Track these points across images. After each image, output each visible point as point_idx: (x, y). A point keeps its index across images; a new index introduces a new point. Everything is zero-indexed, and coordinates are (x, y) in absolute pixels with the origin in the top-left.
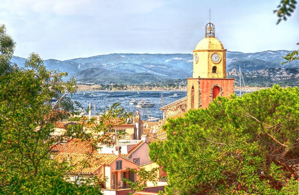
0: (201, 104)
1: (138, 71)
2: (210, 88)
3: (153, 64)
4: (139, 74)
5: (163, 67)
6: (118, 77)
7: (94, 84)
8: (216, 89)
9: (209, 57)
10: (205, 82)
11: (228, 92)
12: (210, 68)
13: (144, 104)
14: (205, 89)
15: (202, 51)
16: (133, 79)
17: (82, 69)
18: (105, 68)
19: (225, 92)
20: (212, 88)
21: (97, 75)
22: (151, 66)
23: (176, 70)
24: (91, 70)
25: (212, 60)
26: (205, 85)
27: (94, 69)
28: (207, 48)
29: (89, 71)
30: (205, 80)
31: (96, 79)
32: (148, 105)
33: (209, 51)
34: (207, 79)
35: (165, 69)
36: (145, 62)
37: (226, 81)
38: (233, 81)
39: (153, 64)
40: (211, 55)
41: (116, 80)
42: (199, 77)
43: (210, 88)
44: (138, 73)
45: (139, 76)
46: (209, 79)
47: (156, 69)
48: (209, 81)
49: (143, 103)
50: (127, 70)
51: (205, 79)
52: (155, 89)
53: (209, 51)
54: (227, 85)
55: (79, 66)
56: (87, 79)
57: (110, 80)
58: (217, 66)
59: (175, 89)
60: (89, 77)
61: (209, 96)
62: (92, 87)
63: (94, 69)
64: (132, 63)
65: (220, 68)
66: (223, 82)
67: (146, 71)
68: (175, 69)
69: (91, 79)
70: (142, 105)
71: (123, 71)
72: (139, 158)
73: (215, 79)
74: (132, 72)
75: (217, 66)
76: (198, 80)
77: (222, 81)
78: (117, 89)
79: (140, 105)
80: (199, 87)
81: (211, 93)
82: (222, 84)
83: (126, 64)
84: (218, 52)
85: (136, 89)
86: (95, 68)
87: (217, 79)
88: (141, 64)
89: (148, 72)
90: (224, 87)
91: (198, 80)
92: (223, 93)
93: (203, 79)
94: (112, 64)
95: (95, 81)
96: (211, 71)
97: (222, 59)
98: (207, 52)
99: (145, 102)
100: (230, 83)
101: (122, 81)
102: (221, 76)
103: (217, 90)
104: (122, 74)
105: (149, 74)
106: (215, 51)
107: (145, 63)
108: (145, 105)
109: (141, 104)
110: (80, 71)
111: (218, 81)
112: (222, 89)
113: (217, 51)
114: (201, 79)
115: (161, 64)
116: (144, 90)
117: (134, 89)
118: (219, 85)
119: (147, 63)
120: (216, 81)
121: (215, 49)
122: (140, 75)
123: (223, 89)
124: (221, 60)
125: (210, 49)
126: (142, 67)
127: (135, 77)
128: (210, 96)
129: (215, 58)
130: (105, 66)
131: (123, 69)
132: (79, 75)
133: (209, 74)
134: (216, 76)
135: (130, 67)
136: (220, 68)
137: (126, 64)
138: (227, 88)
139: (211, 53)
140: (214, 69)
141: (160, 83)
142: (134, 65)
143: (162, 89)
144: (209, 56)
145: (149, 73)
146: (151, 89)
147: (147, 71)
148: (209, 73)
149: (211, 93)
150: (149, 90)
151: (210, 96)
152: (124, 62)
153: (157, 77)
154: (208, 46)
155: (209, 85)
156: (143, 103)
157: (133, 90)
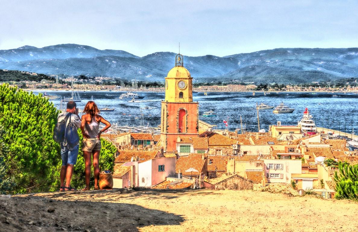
0: (168, 125)
1: (306, 68)
2: (176, 111)
3: (324, 60)
4: (306, 72)
5: (336, 63)
6: (282, 76)
7: (253, 84)
8: (182, 111)
9: (176, 84)
10: (172, 105)
11: (192, 114)
12: (177, 93)
13: (283, 109)
14: (172, 112)
15: (171, 79)
16: (299, 77)
17: (243, 66)
18: (268, 65)
19: (190, 114)
20: (178, 111)
21: (258, 73)
22: (322, 62)
23: (352, 67)
24: (252, 68)
25: (179, 87)
26: (172, 108)
27: (256, 66)
28: (175, 77)
29: (250, 68)
30: (173, 104)
31: (257, 78)
32: (286, 110)
33: (176, 79)
34: (173, 103)
35: (339, 66)
36: (315, 58)
37: (191, 104)
38: (197, 104)
39: (324, 61)
40: (177, 82)
41: (279, 79)
42: (167, 101)
43: (176, 111)
44: (305, 70)
45: (306, 75)
46: (176, 103)
47: (327, 66)
48: (176, 105)
49: (281, 108)
50: (293, 67)
51: (172, 103)
52: (318, 90)
53: (176, 79)
54: (192, 108)
55: (239, 63)
56: (247, 78)
57: (273, 79)
58: (183, 92)
59: (342, 90)
60: (249, 75)
61: (175, 118)
62: (247, 87)
63: (256, 66)
64: (300, 59)
65: (186, 93)
66: (188, 105)
67: (315, 68)
68: (350, 66)
69: (251, 78)
70: (280, 110)
71: (288, 69)
72: (144, 182)
73: (181, 103)
74: (299, 69)
75: (183, 91)
76: (166, 103)
77: (187, 104)
78: (274, 90)
79: (278, 110)
80: (167, 110)
81: (177, 115)
82: (187, 107)
83: (292, 60)
84: (184, 80)
85: (296, 90)
86: (257, 65)
87: (183, 103)
88: (310, 60)
89: (318, 69)
90: (188, 110)
91: (166, 104)
92: (188, 115)
93: (170, 103)
94: (277, 61)
95: (255, 80)
96: (178, 96)
97: (188, 86)
98: (175, 80)
99: (283, 107)
100: (194, 107)
101: (286, 80)
102: (187, 100)
103: (183, 113)
104: (287, 72)
105: (319, 72)
106: (181, 79)
107: (315, 59)
108: (283, 110)
109: (279, 109)
110: (240, 68)
111: (183, 104)
112: (187, 112)
113: (183, 79)
114: (168, 103)
115: (334, 60)
116: (306, 91)
117: (294, 90)
118: (185, 109)
119: (317, 59)
120: (182, 104)
121: (181, 77)
122: (308, 73)
123: (188, 111)
124: (187, 86)
125: (176, 77)
126: (311, 63)
127: (302, 76)
128: (177, 118)
129: (181, 85)
130: (268, 62)
131: (289, 66)
132: (239, 73)
133: (176, 99)
134: (182, 100)
135: (297, 64)
136: (186, 93)
137: (292, 60)
138: (192, 111)
139: (178, 80)
140: (181, 95)
141: (329, 83)
142: (302, 61)
143: (326, 90)
144: (176, 83)
145: (318, 70)
146: (313, 90)
147: (316, 69)
148: (176, 97)
149: (177, 115)
150: (311, 91)
151: (177, 118)
152: (290, 58)
153: (328, 76)
154: (175, 74)
155: (176, 109)
156: (281, 108)
157: (293, 91)
